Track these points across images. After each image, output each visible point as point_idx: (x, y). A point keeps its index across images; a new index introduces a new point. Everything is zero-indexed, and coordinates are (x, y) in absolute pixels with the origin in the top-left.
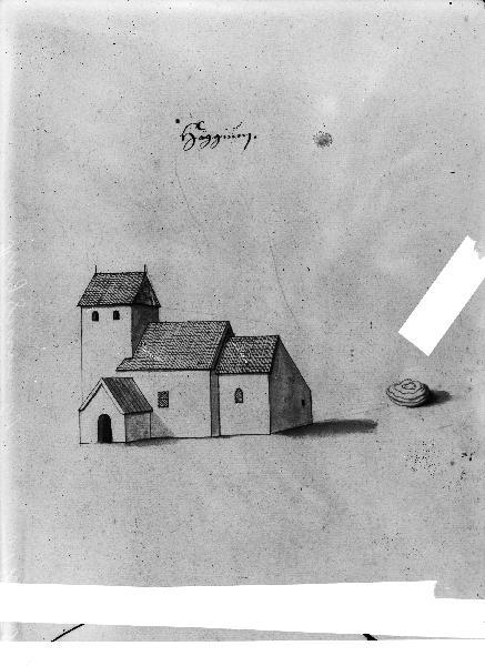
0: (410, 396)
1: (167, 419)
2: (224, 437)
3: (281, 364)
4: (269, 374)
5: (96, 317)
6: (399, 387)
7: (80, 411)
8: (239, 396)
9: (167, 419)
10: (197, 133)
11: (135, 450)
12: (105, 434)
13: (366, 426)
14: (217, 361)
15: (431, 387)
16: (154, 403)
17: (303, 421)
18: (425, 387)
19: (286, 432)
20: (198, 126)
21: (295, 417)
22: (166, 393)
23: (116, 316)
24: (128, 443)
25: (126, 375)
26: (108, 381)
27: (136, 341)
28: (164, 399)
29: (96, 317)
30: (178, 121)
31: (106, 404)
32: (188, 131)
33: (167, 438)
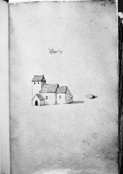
2: (75, 102)
5: (35, 83)
10: (52, 51)
12: (36, 104)
13: (82, 102)
19: (69, 103)
25: (40, 93)
27: (42, 87)
29: (35, 83)
31: (37, 98)
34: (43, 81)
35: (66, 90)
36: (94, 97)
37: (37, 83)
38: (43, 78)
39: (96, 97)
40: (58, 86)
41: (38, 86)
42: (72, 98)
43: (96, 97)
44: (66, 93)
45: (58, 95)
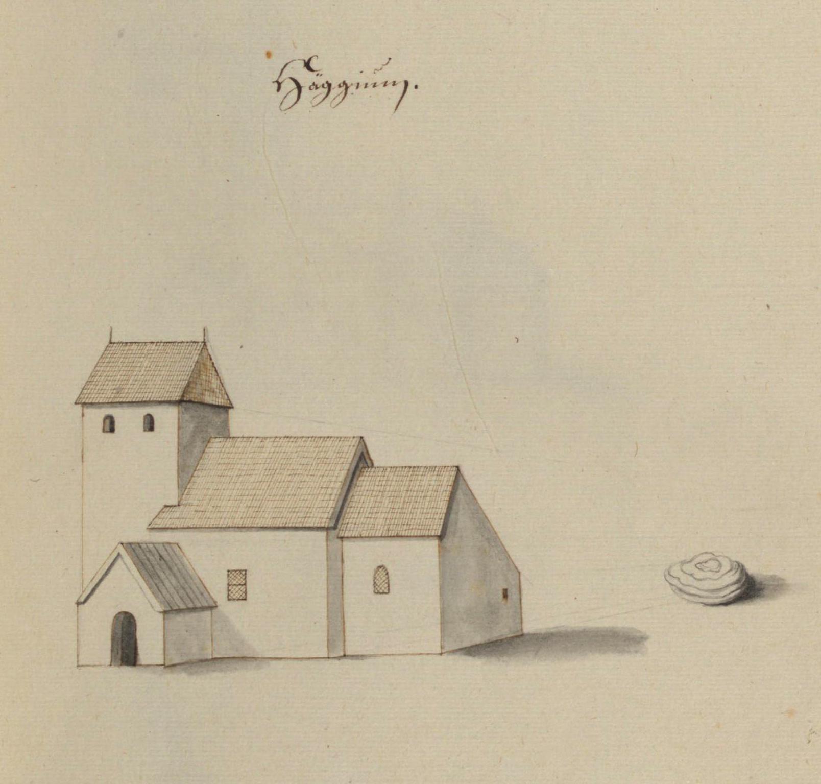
0: (707, 585)
1: (244, 622)
2: (353, 657)
3: (462, 520)
4: (441, 538)
5: (110, 425)
6: (689, 568)
7: (78, 604)
8: (382, 581)
9: (244, 622)
10: (306, 79)
11: (181, 680)
12: (126, 649)
13: (622, 641)
14: (339, 516)
15: (752, 570)
16: (217, 588)
17: (502, 631)
18: (742, 569)
19: (472, 650)
20: (307, 65)
21: (78, 604)
22: (244, 573)
23: (150, 424)
24: (169, 666)
25: (165, 537)
26: (133, 548)
27: (186, 472)
28: (238, 581)
29: (110, 425)
30: (269, 55)
31: (130, 592)
32: (288, 73)
33: (244, 658)
34: (202, 407)
35: (457, 517)
36: (749, 589)
37: (129, 420)
38: (204, 364)
39: (778, 586)
40: (363, 460)
41: (146, 457)
42: (513, 595)
43: (778, 586)
44: (447, 542)
45: (361, 558)
